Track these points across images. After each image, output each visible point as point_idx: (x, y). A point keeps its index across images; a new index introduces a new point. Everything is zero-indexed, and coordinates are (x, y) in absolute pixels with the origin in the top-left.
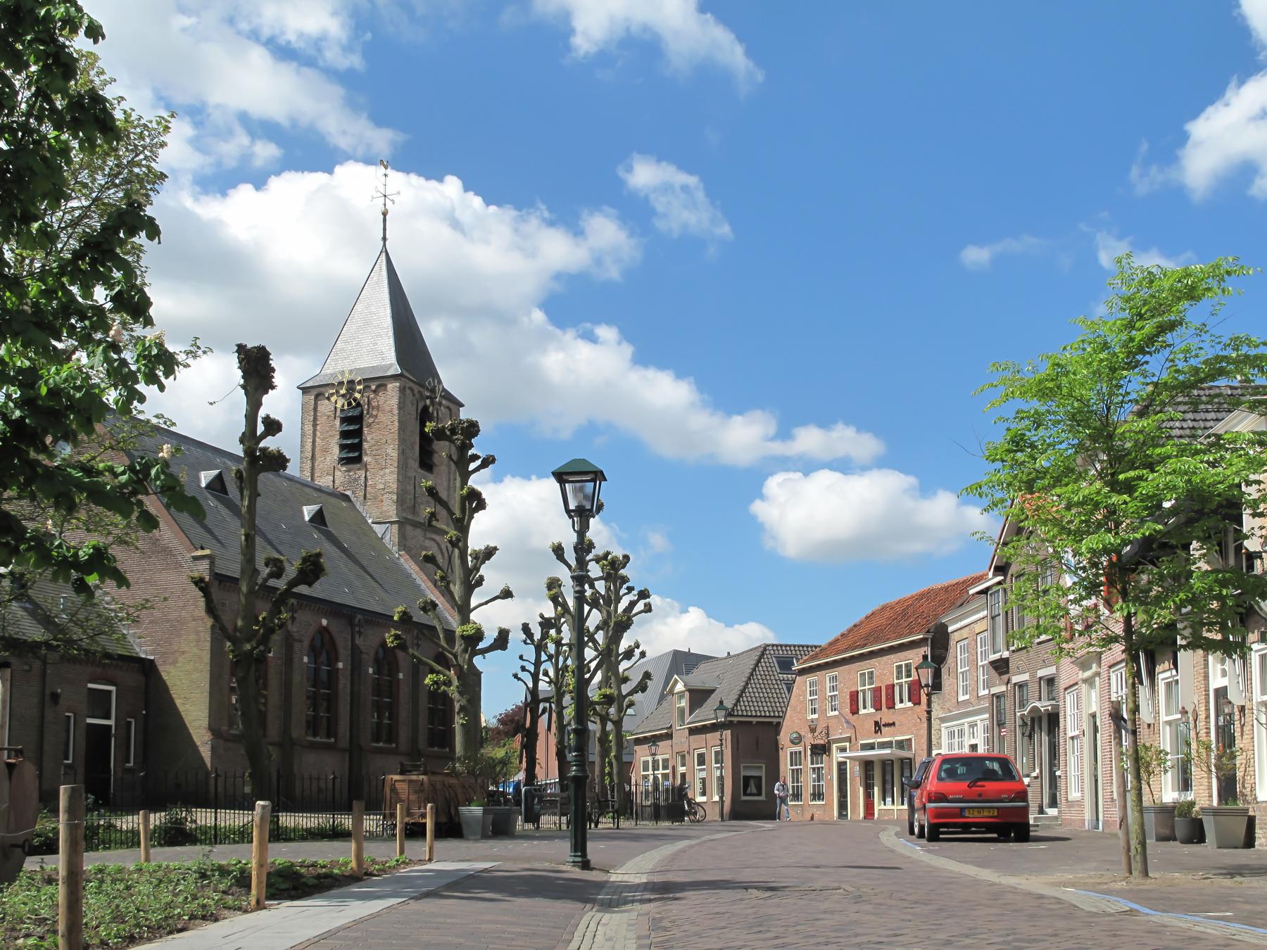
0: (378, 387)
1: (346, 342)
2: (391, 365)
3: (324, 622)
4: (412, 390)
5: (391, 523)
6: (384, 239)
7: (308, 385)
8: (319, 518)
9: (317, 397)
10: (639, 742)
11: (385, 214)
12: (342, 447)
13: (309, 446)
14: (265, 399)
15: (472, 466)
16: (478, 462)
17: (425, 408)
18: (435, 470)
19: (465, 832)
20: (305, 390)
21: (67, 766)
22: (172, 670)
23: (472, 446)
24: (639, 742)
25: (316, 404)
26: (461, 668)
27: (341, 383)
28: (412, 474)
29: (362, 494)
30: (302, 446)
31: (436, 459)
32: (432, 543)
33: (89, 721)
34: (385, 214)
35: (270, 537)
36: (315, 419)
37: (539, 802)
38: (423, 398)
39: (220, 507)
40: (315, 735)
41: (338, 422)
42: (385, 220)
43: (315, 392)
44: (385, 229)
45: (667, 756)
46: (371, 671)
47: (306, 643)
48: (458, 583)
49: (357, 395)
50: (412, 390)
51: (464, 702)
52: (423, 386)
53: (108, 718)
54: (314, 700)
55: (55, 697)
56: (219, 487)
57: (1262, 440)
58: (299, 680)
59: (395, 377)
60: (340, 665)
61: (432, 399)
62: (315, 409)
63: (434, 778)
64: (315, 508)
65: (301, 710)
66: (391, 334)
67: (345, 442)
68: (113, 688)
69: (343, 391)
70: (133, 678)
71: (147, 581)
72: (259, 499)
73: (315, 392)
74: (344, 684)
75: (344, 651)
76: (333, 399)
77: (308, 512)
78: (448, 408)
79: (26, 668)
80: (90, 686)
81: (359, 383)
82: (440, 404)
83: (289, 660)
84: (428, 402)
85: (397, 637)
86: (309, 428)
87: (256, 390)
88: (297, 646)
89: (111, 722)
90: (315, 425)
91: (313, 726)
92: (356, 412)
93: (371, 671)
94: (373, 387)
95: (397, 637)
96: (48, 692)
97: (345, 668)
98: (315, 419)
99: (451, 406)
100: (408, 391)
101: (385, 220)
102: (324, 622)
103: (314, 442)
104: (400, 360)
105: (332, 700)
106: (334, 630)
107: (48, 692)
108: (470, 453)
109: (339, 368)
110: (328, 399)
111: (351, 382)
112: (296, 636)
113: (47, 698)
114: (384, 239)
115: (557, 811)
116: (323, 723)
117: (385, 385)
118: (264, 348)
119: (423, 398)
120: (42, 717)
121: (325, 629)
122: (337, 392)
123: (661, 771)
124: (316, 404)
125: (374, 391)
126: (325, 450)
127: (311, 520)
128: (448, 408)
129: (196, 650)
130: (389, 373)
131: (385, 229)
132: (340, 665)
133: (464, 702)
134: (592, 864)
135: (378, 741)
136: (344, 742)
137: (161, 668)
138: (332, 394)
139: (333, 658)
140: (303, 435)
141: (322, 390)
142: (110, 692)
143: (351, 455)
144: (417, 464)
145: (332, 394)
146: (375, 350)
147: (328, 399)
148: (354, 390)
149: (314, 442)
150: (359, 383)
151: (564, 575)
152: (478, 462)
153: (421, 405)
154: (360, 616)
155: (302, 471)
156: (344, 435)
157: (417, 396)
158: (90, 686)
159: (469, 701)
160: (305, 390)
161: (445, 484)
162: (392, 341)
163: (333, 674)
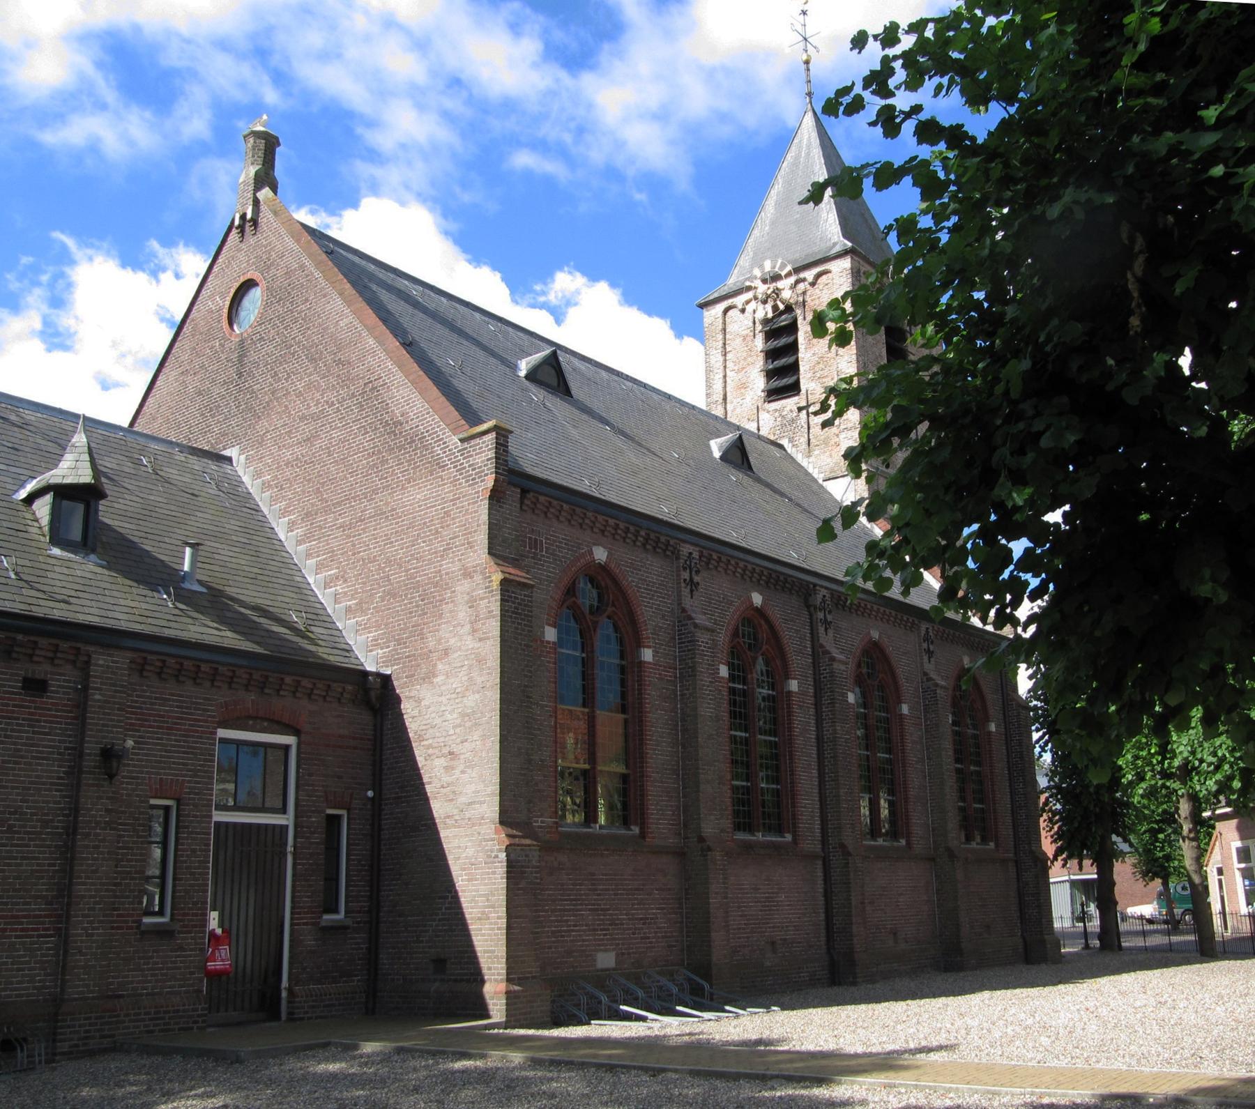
3: (757, 599)
12: (770, 374)
13: (718, 386)
29: (804, 440)
30: (709, 386)
33: (219, 817)
41: (760, 339)
46: (851, 698)
47: (723, 638)
53: (284, 810)
54: (742, 760)
55: (110, 756)
56: (554, 382)
57: (1, 957)
58: (711, 709)
60: (794, 685)
70: (343, 720)
71: (380, 513)
74: (803, 720)
75: (799, 661)
76: (750, 308)
77: (716, 447)
83: (686, 671)
91: (748, 812)
92: (784, 321)
93: (851, 698)
96: (92, 748)
97: (802, 693)
102: (757, 599)
104: (847, 232)
105: (779, 761)
106: (776, 614)
107: (92, 748)
112: (700, 619)
116: (763, 809)
120: (75, 810)
121: (759, 611)
129: (470, 643)
132: (794, 685)
136: (811, 844)
139: (778, 672)
140: (709, 370)
156: (771, 355)
163: (779, 704)
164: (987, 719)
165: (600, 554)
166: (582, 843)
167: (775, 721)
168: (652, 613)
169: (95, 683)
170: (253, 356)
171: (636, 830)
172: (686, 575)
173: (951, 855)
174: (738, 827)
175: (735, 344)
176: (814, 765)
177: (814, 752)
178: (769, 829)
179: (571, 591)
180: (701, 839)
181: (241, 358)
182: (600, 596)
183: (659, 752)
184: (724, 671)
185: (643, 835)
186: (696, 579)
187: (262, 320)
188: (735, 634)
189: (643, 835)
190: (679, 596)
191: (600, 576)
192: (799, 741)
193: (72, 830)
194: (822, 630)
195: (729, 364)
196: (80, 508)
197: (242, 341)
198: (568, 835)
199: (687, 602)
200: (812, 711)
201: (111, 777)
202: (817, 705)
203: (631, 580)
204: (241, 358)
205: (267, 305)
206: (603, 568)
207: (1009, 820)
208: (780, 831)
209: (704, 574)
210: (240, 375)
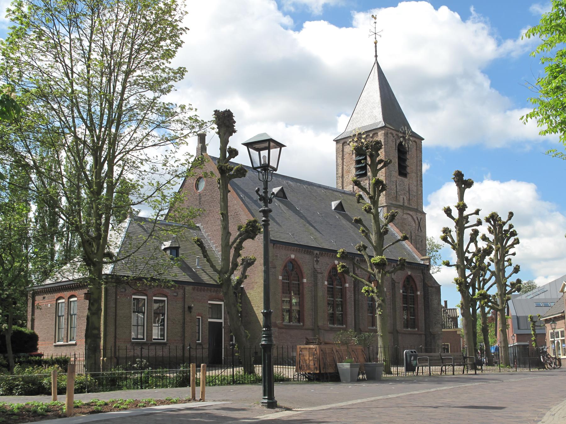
0: (374, 134)
1: (358, 113)
2: (380, 122)
4: (392, 134)
5: (383, 207)
6: (376, 56)
7: (339, 138)
8: (340, 207)
9: (343, 144)
10: (547, 321)
11: (376, 43)
12: (357, 169)
13: (340, 171)
14: (230, 138)
15: (380, 166)
16: (382, 164)
17: (400, 144)
18: (408, 176)
19: (341, 378)
20: (337, 141)
21: (200, 344)
22: (251, 292)
23: (379, 155)
24: (547, 321)
25: (343, 148)
26: (378, 282)
27: (354, 135)
28: (394, 179)
30: (337, 171)
31: (408, 170)
32: (409, 216)
33: (210, 320)
34: (376, 43)
35: (309, 219)
36: (343, 156)
37: (415, 359)
38: (399, 137)
39: (281, 205)
40: (333, 324)
41: (354, 156)
42: (376, 46)
43: (342, 142)
44: (376, 51)
45: (562, 329)
47: (326, 274)
48: (374, 233)
49: (363, 141)
50: (392, 134)
51: (380, 302)
52: (398, 131)
53: (221, 319)
55: (190, 308)
56: (282, 196)
58: (322, 293)
59: (381, 128)
60: (347, 285)
61: (404, 138)
62: (343, 151)
63: (323, 346)
64: (338, 202)
65: (324, 310)
66: (380, 105)
67: (358, 166)
68: (222, 303)
69: (356, 139)
72: (229, 194)
73: (342, 142)
77: (334, 204)
78: (415, 141)
79: (175, 294)
80: (209, 302)
81: (364, 134)
82: (409, 139)
84: (402, 139)
85: (343, 267)
86: (340, 161)
87: (225, 134)
88: (319, 276)
89: (222, 321)
90: (343, 159)
91: (332, 318)
94: (371, 135)
95: (343, 267)
96: (186, 307)
98: (343, 156)
99: (417, 140)
100: (390, 135)
101: (376, 46)
103: (343, 168)
107: (186, 307)
108: (378, 159)
109: (354, 127)
110: (349, 144)
111: (360, 134)
112: (319, 271)
113: (186, 309)
114: (376, 56)
115: (428, 364)
117: (377, 133)
118: (229, 111)
119: (399, 137)
120: (184, 319)
122: (353, 140)
123: (560, 338)
124: (343, 148)
125: (372, 137)
126: (349, 172)
127: (335, 209)
128: (415, 141)
130: (379, 127)
131: (376, 51)
132: (347, 285)
133: (380, 302)
134: (279, 403)
135: (407, 327)
137: (247, 291)
138: (350, 142)
140: (337, 165)
141: (346, 140)
142: (221, 305)
143: (361, 173)
144: (397, 174)
145: (350, 142)
146: (370, 114)
147: (349, 144)
148: (361, 138)
149: (343, 168)
150: (364, 134)
151: (452, 225)
152: (382, 164)
153: (398, 142)
154: (357, 258)
155: (337, 184)
156: (358, 162)
157: (396, 137)
158: (209, 302)
159: (382, 301)
160: (337, 141)
161: (415, 183)
162: (380, 110)
163: (343, 292)
164: (417, 291)
165: (293, 256)
166: (288, 327)
167: (342, 295)
168: (306, 270)
169: (186, 293)
170: (203, 199)
171: (302, 324)
172: (316, 259)
173: (397, 332)
174: (404, 327)
175: (346, 156)
176: (353, 307)
177: (353, 303)
178: (411, 328)
179: (285, 266)
180: (318, 326)
181: (200, 199)
182: (293, 266)
183: (308, 304)
184: (326, 283)
185: (303, 325)
186: (318, 259)
187: (205, 189)
188: (330, 272)
189: (303, 325)
190: (314, 265)
191: (292, 261)
192: (348, 300)
193: (184, 323)
194: (356, 269)
195: (345, 163)
196: (175, 251)
197: (200, 194)
198: (285, 325)
199: (315, 266)
200: (353, 292)
201: (191, 312)
202: (354, 290)
203: (300, 262)
204: (200, 199)
205: (206, 185)
206: (293, 260)
207: (423, 322)
208: (342, 324)
209: (321, 258)
210: (200, 204)
